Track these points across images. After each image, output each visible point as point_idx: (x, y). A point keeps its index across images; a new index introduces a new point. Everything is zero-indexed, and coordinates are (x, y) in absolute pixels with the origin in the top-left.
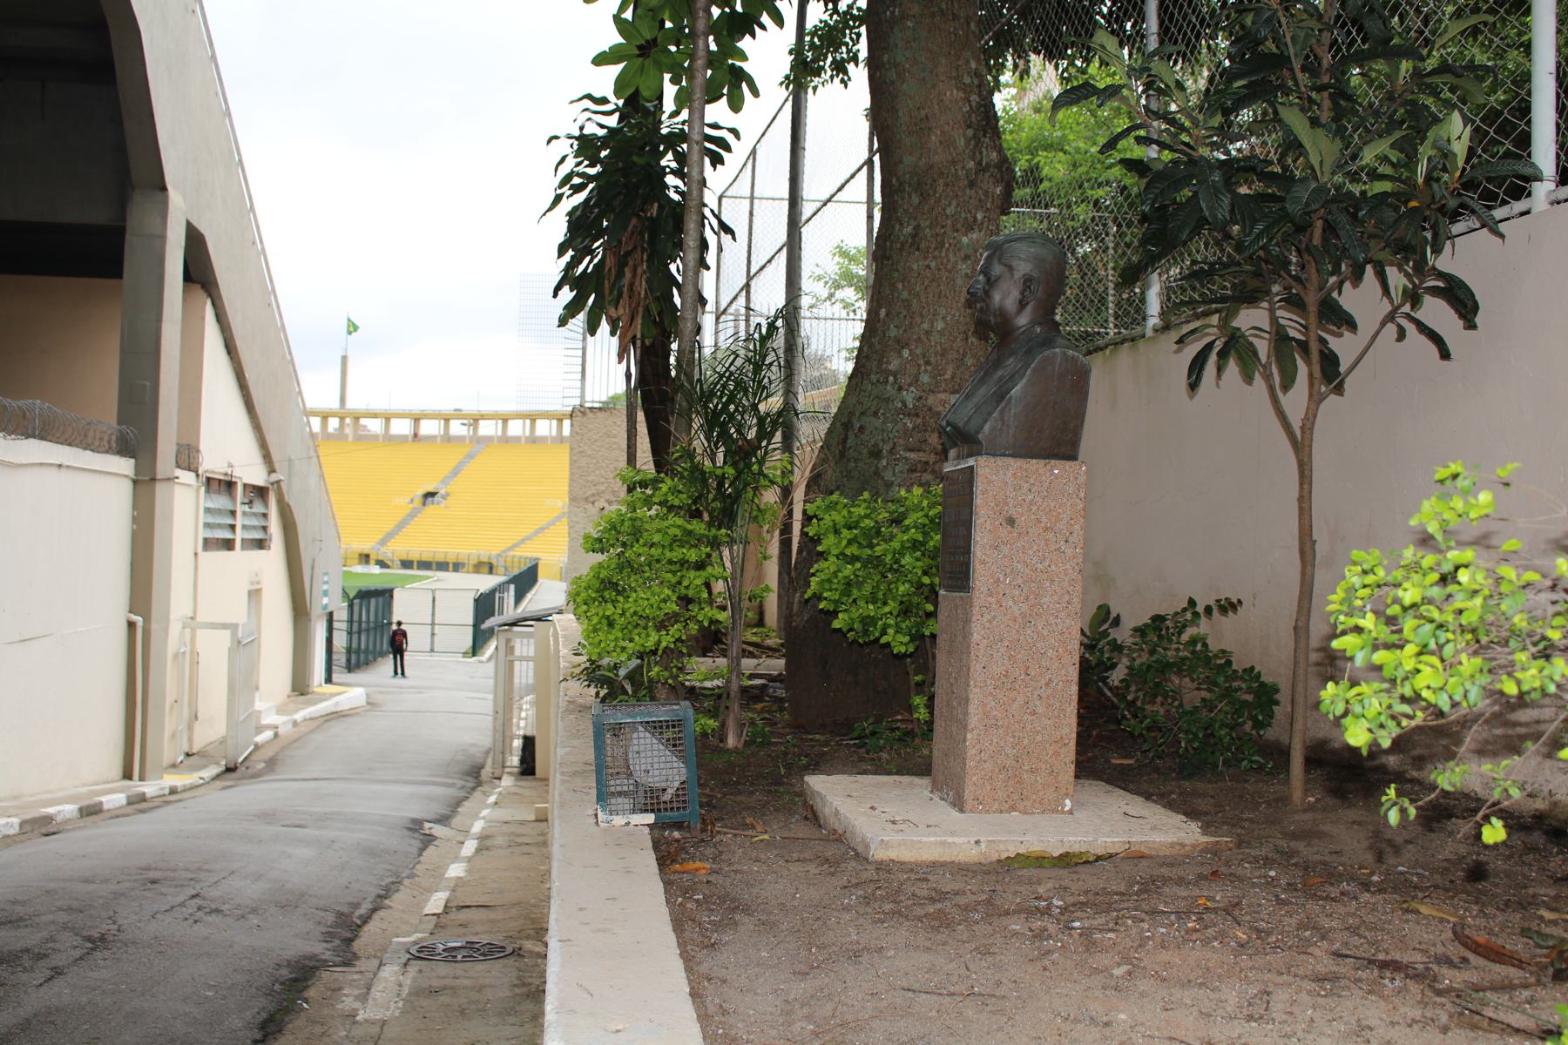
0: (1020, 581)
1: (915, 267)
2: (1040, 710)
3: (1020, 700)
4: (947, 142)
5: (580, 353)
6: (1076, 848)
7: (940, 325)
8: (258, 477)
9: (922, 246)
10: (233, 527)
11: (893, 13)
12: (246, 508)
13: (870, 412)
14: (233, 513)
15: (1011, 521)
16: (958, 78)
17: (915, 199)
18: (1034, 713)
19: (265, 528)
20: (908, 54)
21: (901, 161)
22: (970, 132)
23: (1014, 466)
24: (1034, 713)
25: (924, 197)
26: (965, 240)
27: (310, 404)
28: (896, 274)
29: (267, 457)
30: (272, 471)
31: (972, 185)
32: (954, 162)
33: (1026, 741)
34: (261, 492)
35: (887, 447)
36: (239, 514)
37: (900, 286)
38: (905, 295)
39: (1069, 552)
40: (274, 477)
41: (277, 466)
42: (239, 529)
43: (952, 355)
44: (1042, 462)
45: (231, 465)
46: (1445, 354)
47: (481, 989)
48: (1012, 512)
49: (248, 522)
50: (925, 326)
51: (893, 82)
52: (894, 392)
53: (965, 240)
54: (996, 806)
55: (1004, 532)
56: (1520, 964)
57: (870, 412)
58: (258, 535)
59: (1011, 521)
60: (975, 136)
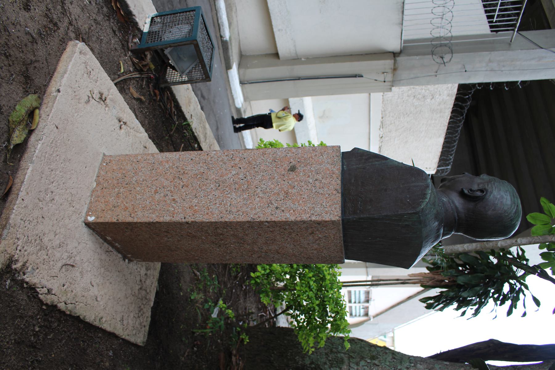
0: (249, 178)
2: (157, 197)
3: (166, 183)
5: (405, 13)
8: (371, 313)
10: (355, 303)
12: (361, 307)
13: (394, 356)
14: (359, 302)
15: (293, 169)
18: (156, 192)
19: (356, 316)
24: (156, 192)
27: (395, 332)
29: (377, 315)
30: (374, 317)
33: (138, 189)
34: (366, 314)
35: (376, 362)
36: (359, 304)
39: (269, 211)
40: (372, 318)
41: (375, 318)
42: (355, 304)
44: (339, 187)
45: (374, 300)
47: (114, 32)
48: (300, 169)
49: (358, 308)
52: (405, 365)
54: (102, 173)
57: (394, 356)
58: (354, 314)
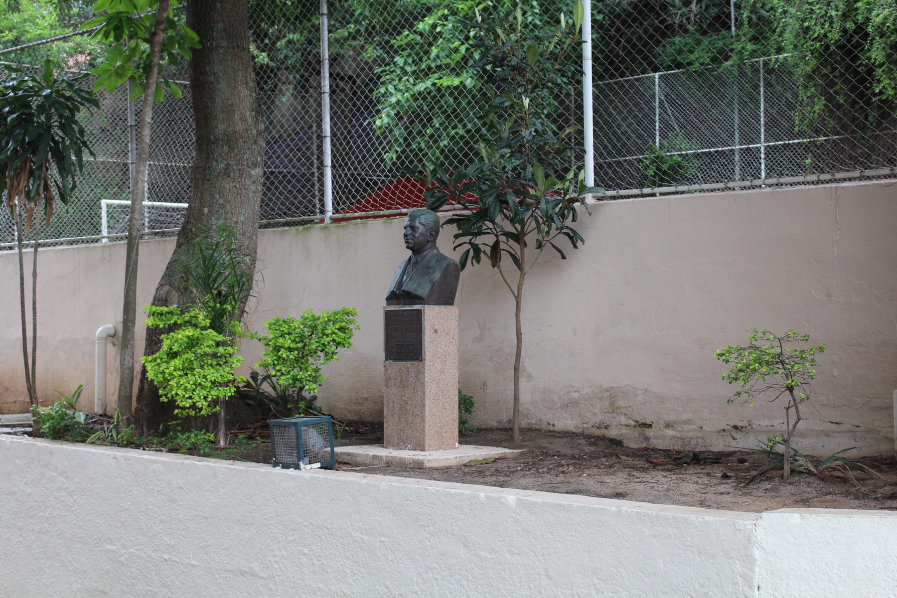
1: (227, 186)
4: (243, 119)
6: (473, 458)
7: (242, 219)
9: (232, 175)
11: (211, 44)
16: (247, 83)
17: (226, 148)
20: (221, 68)
21: (216, 127)
22: (253, 113)
23: (437, 308)
25: (232, 148)
26: (253, 172)
28: (214, 190)
31: (255, 142)
32: (247, 130)
37: (217, 197)
38: (221, 201)
43: (247, 235)
46: (564, 257)
48: (437, 327)
50: (235, 219)
51: (212, 83)
53: (253, 172)
55: (434, 335)
56: (794, 427)
59: (436, 331)
60: (256, 116)
